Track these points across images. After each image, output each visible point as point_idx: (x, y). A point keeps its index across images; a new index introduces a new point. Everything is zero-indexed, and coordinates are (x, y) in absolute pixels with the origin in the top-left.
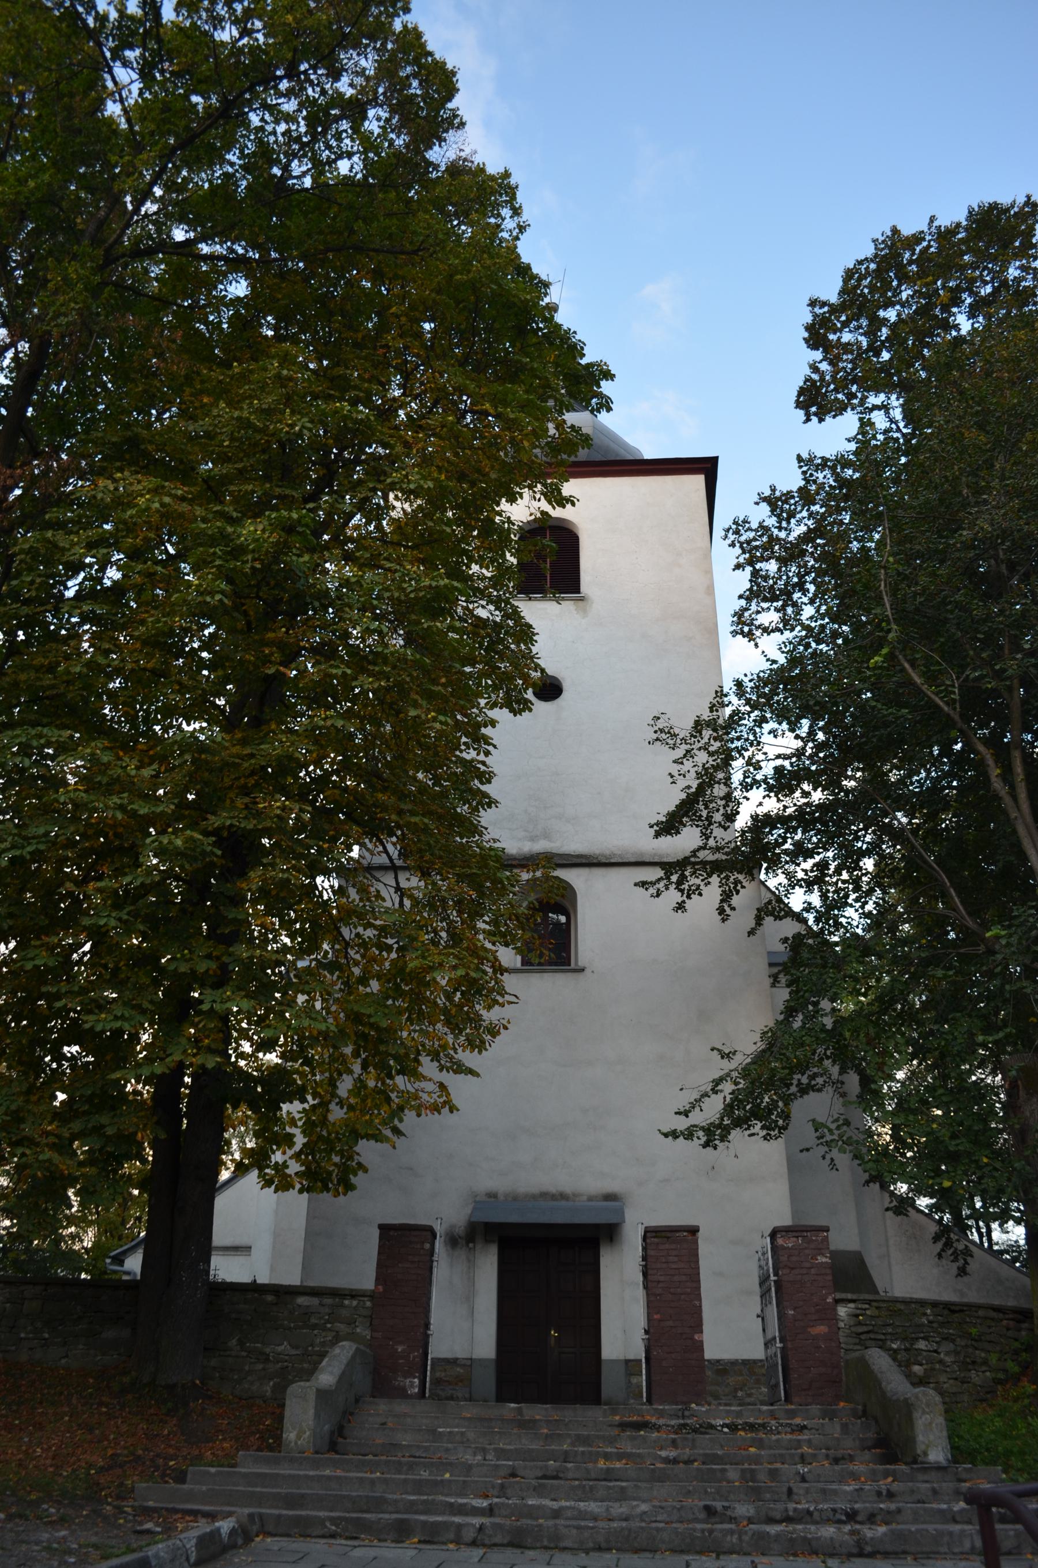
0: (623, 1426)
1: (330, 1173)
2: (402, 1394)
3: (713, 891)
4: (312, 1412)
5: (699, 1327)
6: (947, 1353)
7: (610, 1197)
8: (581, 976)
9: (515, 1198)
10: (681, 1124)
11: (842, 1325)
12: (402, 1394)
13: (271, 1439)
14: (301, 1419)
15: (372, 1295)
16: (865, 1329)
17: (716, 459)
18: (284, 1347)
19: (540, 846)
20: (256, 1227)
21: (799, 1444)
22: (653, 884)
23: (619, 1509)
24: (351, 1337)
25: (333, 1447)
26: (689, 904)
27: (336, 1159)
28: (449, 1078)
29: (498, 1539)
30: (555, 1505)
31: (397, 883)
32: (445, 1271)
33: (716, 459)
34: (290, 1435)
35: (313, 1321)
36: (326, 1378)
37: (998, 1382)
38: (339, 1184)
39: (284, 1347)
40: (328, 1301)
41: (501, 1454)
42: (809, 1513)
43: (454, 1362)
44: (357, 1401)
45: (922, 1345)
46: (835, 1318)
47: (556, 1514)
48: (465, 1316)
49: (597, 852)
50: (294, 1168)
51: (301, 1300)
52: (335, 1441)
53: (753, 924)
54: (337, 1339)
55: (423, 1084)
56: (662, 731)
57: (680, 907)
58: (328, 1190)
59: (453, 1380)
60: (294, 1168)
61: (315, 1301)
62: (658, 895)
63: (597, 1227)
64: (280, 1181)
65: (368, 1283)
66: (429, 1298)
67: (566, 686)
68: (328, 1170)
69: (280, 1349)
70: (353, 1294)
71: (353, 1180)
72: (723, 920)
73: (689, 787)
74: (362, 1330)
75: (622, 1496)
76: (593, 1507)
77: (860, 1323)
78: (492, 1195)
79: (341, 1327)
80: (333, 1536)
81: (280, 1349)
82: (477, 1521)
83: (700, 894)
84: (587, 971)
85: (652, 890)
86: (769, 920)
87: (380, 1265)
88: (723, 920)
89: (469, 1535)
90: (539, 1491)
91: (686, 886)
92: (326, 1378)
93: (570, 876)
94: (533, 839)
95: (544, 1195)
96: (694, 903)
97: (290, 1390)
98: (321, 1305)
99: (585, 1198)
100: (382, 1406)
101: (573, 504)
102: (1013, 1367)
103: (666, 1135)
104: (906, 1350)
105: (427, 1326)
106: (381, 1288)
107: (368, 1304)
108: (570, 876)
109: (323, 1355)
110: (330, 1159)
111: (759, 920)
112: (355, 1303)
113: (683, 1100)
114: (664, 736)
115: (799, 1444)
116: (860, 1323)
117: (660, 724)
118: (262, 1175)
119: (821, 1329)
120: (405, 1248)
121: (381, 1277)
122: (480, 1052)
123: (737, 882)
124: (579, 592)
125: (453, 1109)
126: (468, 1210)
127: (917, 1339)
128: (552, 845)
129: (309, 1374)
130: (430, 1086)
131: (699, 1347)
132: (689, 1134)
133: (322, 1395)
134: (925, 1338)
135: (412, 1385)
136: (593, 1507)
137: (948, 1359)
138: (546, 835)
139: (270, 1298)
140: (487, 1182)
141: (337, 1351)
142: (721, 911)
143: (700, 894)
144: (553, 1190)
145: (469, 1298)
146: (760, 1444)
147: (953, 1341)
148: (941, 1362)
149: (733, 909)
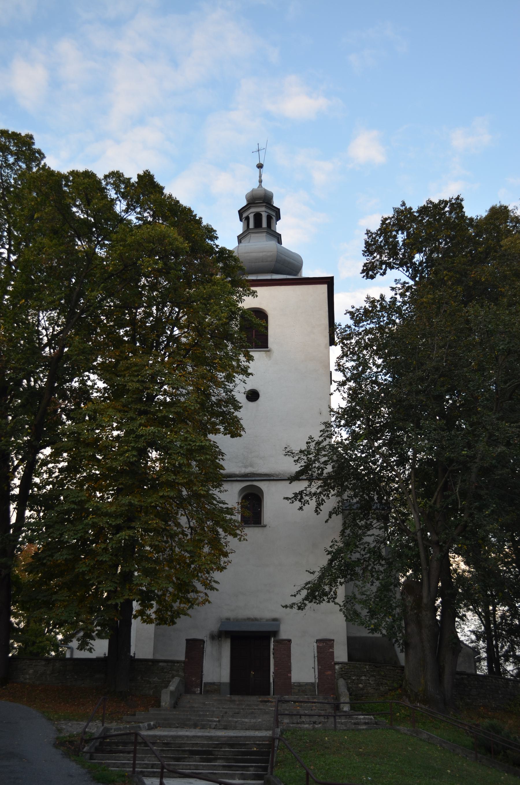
0: (261, 701)
1: (167, 618)
2: (194, 693)
3: (313, 503)
4: (169, 697)
5: (290, 671)
6: (372, 681)
7: (275, 620)
8: (265, 529)
9: (237, 621)
10: (289, 602)
11: (336, 671)
12: (194, 693)
13: (157, 704)
14: (166, 700)
15: (184, 662)
16: (344, 672)
17: (333, 277)
18: (156, 679)
19: (249, 470)
20: (143, 639)
21: (313, 706)
22: (290, 499)
23: (253, 721)
24: (178, 676)
25: (175, 707)
26: (304, 508)
27: (169, 613)
28: (208, 592)
29: (220, 727)
30: (236, 720)
31: (190, 525)
32: (209, 649)
33: (333, 277)
34: (163, 704)
35: (165, 670)
36: (172, 687)
37: (390, 690)
38: (170, 622)
39: (156, 679)
40: (170, 664)
41: (223, 708)
42: (303, 722)
43: (214, 684)
44: (181, 695)
45: (363, 678)
46: (334, 669)
47: (236, 722)
48: (217, 667)
49: (273, 473)
50: (153, 616)
51: (161, 664)
52: (175, 706)
53: (327, 517)
54: (173, 677)
55: (199, 594)
56: (288, 452)
57: (301, 508)
58: (166, 624)
59: (214, 689)
60: (153, 616)
61: (165, 664)
62: (293, 503)
63: (269, 632)
64: (148, 620)
65: (182, 658)
66: (203, 663)
67: (261, 394)
68: (166, 618)
69: (154, 680)
70: (178, 662)
71: (175, 620)
72: (318, 514)
73: (302, 466)
74: (181, 674)
75: (255, 717)
76: (246, 720)
77: (342, 671)
78: (228, 619)
79: (174, 672)
80: (177, 727)
81: (154, 680)
82: (215, 723)
83: (309, 504)
84: (268, 527)
85: (290, 501)
86: (334, 516)
87: (186, 653)
88: (318, 514)
89: (213, 726)
90: (233, 716)
91: (303, 500)
92: (172, 687)
93: (263, 486)
94: (246, 467)
95: (249, 619)
96: (306, 507)
97: (162, 692)
98: (167, 665)
99: (265, 620)
100: (188, 696)
101: (252, 375)
102: (395, 685)
103: (283, 607)
104: (357, 679)
105: (202, 672)
106: (187, 660)
107: (183, 665)
108: (263, 486)
109: (170, 681)
110: (167, 613)
111: (330, 517)
112: (178, 665)
113: (294, 591)
114: (289, 454)
115: (313, 706)
116: (342, 671)
117: (288, 450)
118: (142, 619)
119: (329, 673)
120: (195, 647)
121: (186, 657)
122: (221, 572)
123: (323, 500)
124: (268, 348)
125: (209, 602)
126: (219, 625)
127: (362, 676)
128: (254, 469)
129: (166, 687)
130: (202, 595)
131: (290, 678)
132: (291, 607)
133: (172, 693)
134: (365, 676)
135: (197, 691)
136: (246, 720)
137: (372, 683)
138: (251, 466)
139: (150, 663)
140: (227, 614)
141: (174, 680)
142: (316, 511)
143: (309, 504)
144: (252, 617)
145: (219, 659)
146: (301, 707)
147: (375, 677)
148: (369, 683)
149: (321, 510)
